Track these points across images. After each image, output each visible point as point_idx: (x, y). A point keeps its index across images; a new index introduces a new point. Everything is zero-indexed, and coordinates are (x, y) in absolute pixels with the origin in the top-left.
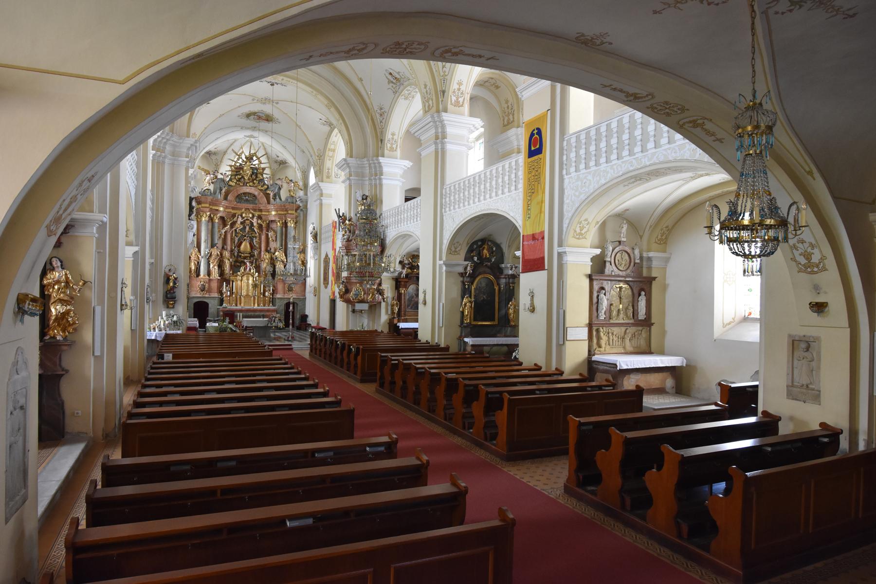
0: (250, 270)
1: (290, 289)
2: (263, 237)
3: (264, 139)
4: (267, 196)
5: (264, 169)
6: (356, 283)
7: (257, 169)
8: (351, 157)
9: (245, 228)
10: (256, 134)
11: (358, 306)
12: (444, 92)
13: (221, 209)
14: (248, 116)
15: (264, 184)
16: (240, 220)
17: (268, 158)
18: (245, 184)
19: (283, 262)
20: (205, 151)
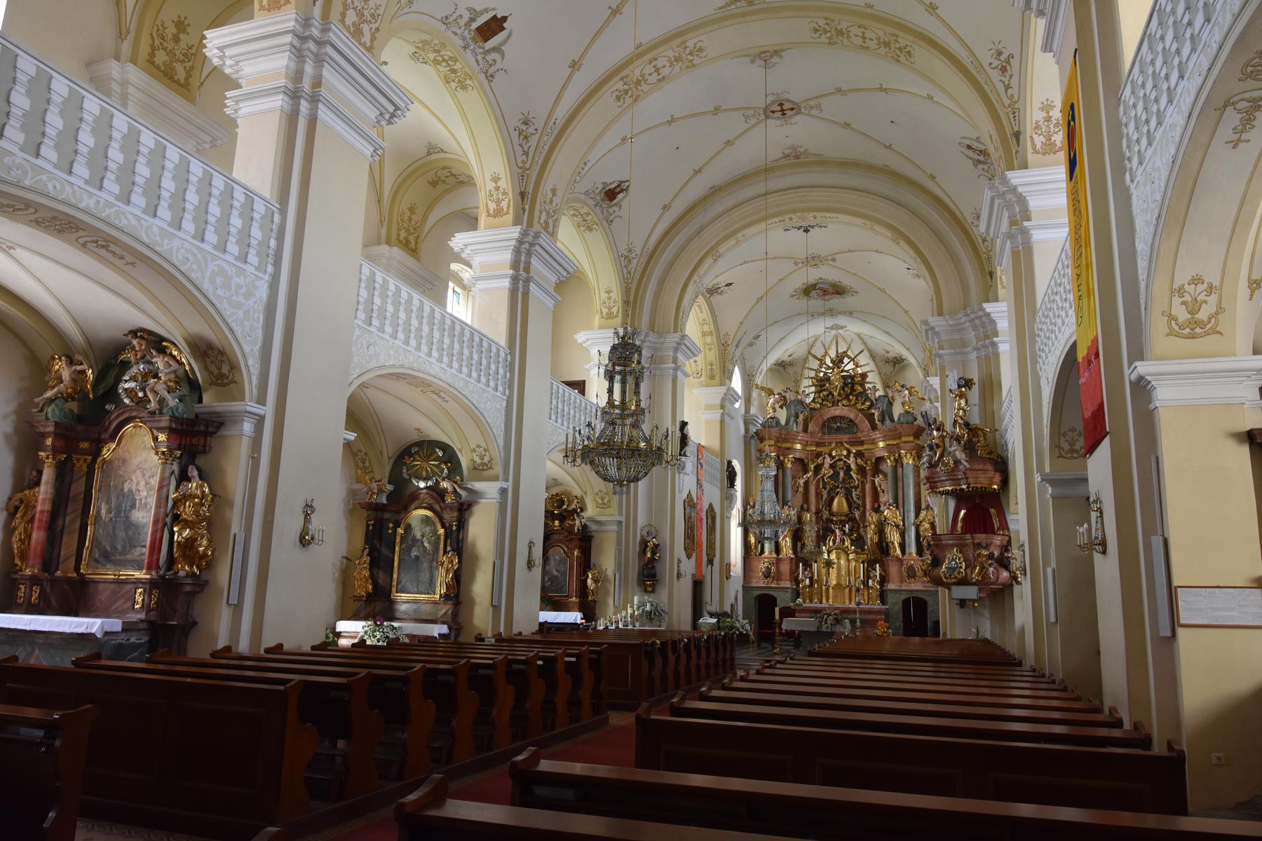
0: (843, 541)
1: (911, 573)
2: (868, 487)
3: (854, 327)
4: (870, 418)
5: (864, 376)
6: (952, 546)
7: (852, 377)
8: (940, 313)
9: (836, 474)
10: (841, 320)
12: (1017, 135)
13: (798, 446)
14: (808, 290)
15: (867, 399)
16: (828, 461)
17: (873, 356)
18: (835, 403)
19: (897, 526)
20: (772, 359)
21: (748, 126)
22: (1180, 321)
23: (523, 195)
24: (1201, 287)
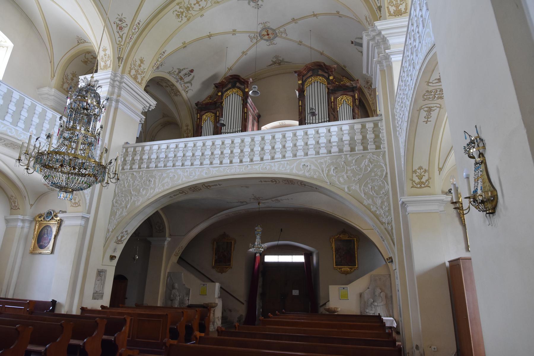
12: (380, 8)
21: (253, 44)
22: (416, 182)
23: (119, 58)
24: (422, 170)
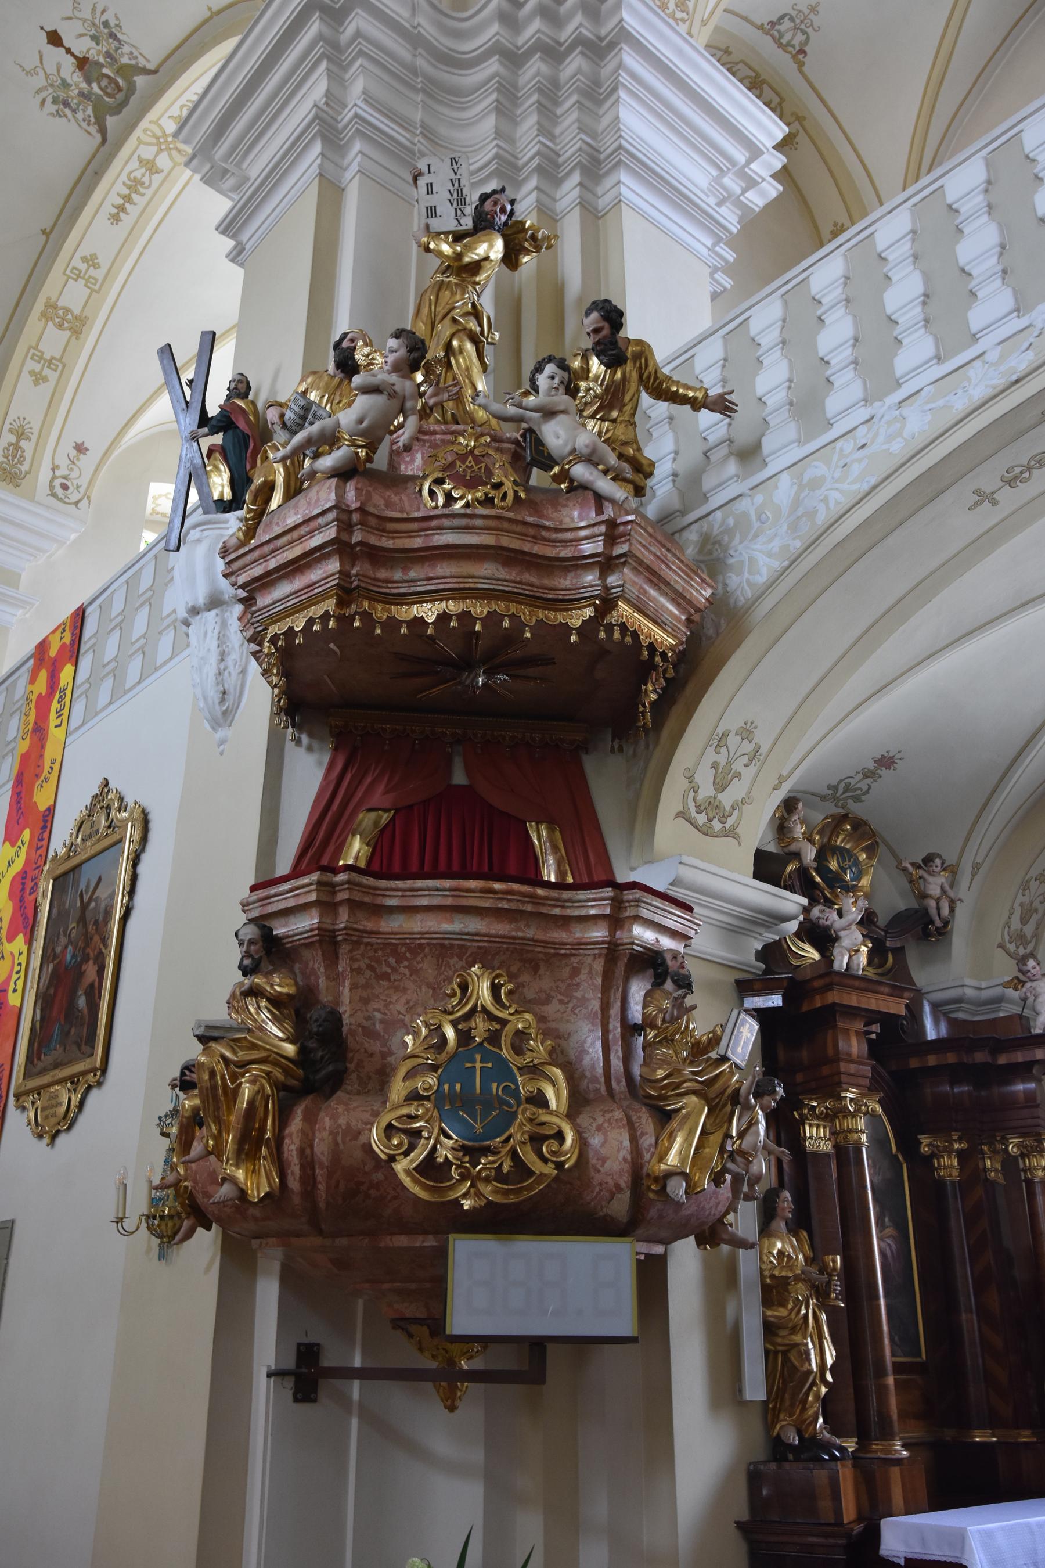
11: (495, 1288)
22: (700, 797)
